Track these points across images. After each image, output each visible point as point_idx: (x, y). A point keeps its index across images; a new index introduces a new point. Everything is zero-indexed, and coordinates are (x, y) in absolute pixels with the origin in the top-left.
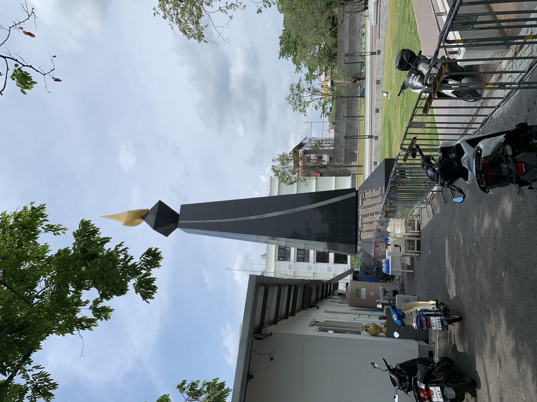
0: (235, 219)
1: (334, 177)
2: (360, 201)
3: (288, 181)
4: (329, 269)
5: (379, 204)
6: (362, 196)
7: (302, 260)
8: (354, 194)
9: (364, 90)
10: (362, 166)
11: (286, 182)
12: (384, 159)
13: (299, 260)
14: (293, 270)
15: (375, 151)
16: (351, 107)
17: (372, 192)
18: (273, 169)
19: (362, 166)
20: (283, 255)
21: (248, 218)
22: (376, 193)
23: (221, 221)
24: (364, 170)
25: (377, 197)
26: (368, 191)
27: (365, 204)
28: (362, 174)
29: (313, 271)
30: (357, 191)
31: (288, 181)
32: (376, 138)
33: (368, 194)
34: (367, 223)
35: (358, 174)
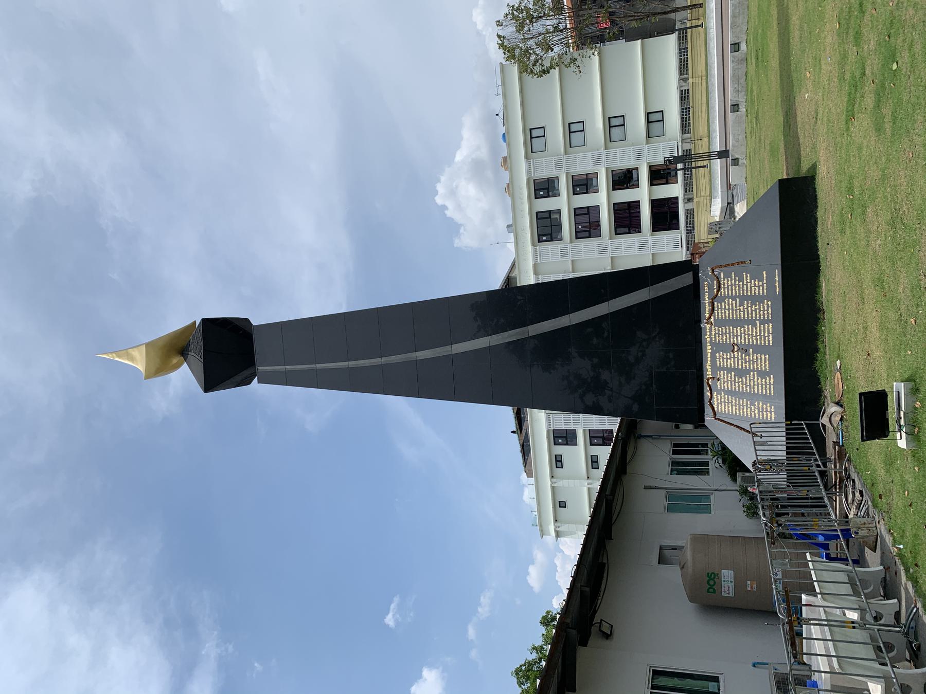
0: (384, 360)
1: (639, 42)
3: (537, 68)
4: (643, 247)
5: (763, 322)
6: (710, 287)
7: (587, 234)
8: (686, 279)
10: (701, 5)
11: (532, 72)
12: (776, 180)
13: (580, 235)
14: (569, 258)
15: (734, 16)
17: (741, 280)
18: (502, 46)
19: (701, 5)
20: (548, 231)
21: (413, 356)
22: (758, 288)
23: (352, 364)
24: (704, 14)
25: (755, 299)
26: (728, 276)
27: (722, 312)
28: (701, 26)
29: (609, 254)
31: (537, 68)
33: (730, 285)
34: (729, 370)
35: (691, 27)
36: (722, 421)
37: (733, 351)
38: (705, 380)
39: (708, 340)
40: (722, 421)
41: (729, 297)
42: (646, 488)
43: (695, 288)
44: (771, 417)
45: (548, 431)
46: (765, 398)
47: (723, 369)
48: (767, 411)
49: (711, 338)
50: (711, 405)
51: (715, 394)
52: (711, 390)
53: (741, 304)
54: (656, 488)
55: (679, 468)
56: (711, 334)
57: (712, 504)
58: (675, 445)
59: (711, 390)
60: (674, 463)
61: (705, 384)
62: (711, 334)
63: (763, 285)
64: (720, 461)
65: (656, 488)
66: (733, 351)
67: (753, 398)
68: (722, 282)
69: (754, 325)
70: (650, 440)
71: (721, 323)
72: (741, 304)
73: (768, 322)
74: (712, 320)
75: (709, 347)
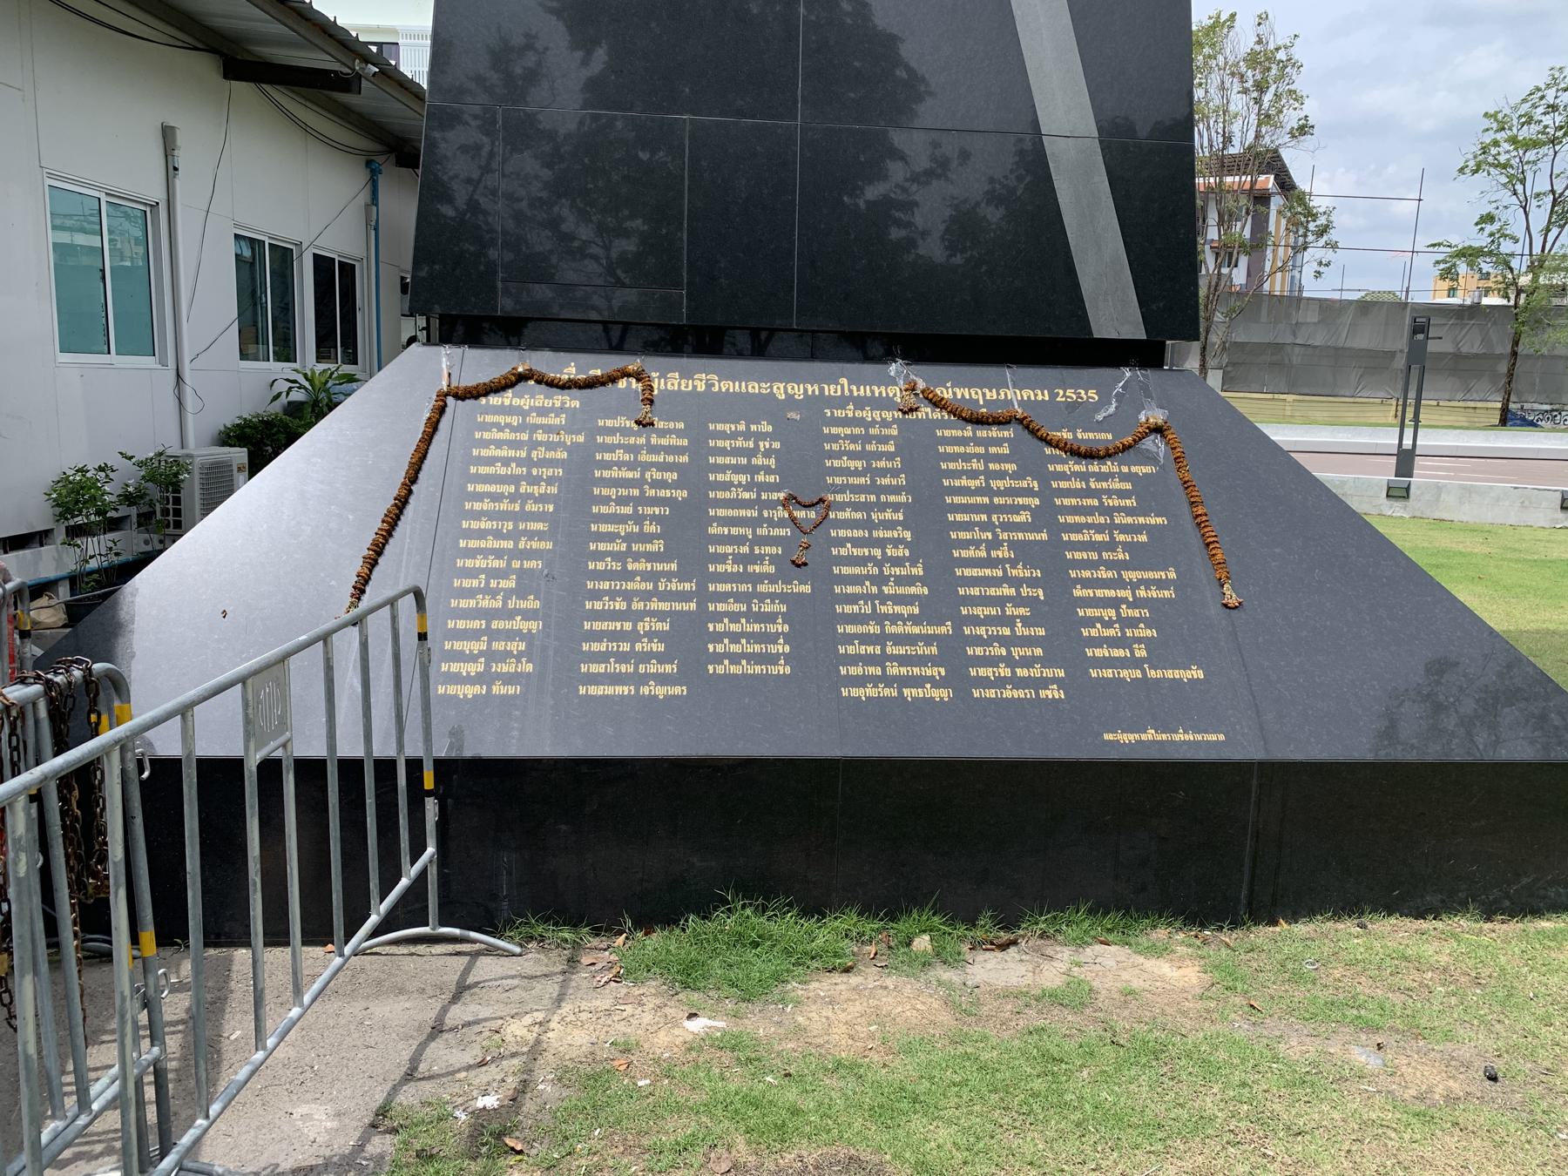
2: (1015, 390)
5: (953, 654)
8: (1114, 311)
9: (1532, 424)
16: (1464, 370)
17: (1141, 557)
22: (1119, 645)
26: (1146, 495)
27: (975, 464)
30: (1146, 354)
32: (1399, 493)
33: (1109, 505)
34: (695, 476)
36: (433, 426)
37: (792, 500)
38: (634, 363)
39: (830, 390)
40: (433, 426)
41: (1047, 494)
42: (167, 134)
43: (1086, 352)
44: (459, 681)
45: (394, 31)
46: (561, 647)
47: (699, 446)
48: (491, 656)
49: (842, 402)
50: (514, 380)
51: (572, 401)
52: (590, 384)
53: (1023, 553)
54: (171, 170)
55: (262, 271)
56: (860, 403)
57: (113, 357)
58: (348, 270)
59: (590, 384)
60: (284, 257)
61: (614, 362)
62: (860, 403)
63: (1135, 663)
64: (298, 396)
65: (171, 170)
66: (792, 500)
67: (564, 585)
68: (1109, 466)
69: (931, 611)
70: (364, 197)
71: (919, 456)
72: (1023, 553)
73: (958, 679)
74: (926, 412)
75: (797, 391)
